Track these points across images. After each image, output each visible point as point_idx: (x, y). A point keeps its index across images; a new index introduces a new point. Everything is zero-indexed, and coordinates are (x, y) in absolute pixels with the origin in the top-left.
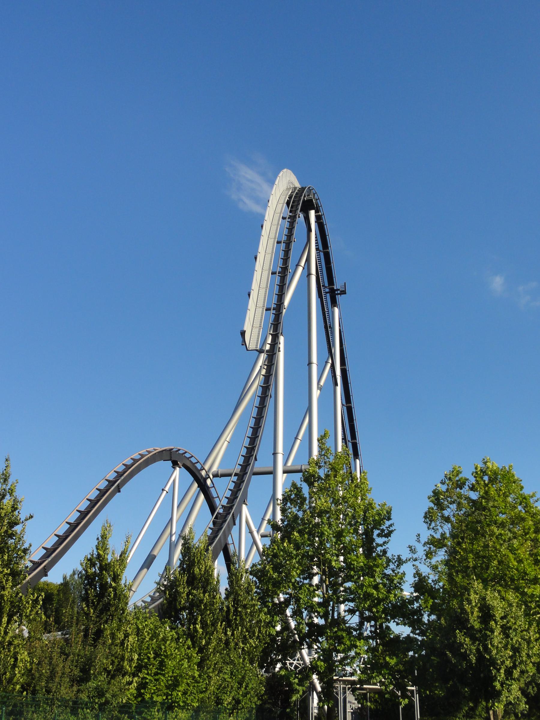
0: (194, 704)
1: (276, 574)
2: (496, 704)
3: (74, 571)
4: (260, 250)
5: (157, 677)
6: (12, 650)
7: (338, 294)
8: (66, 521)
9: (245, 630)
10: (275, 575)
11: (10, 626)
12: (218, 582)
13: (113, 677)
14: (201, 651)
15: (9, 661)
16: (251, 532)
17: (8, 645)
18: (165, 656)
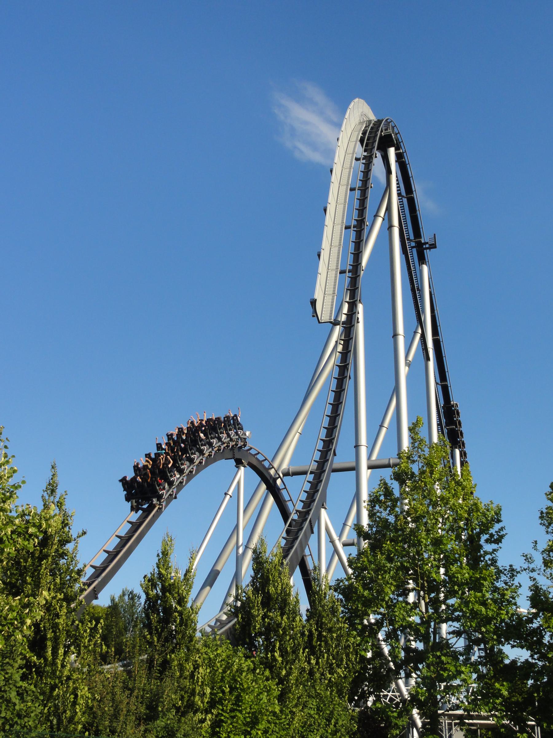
4: (330, 201)
7: (426, 249)
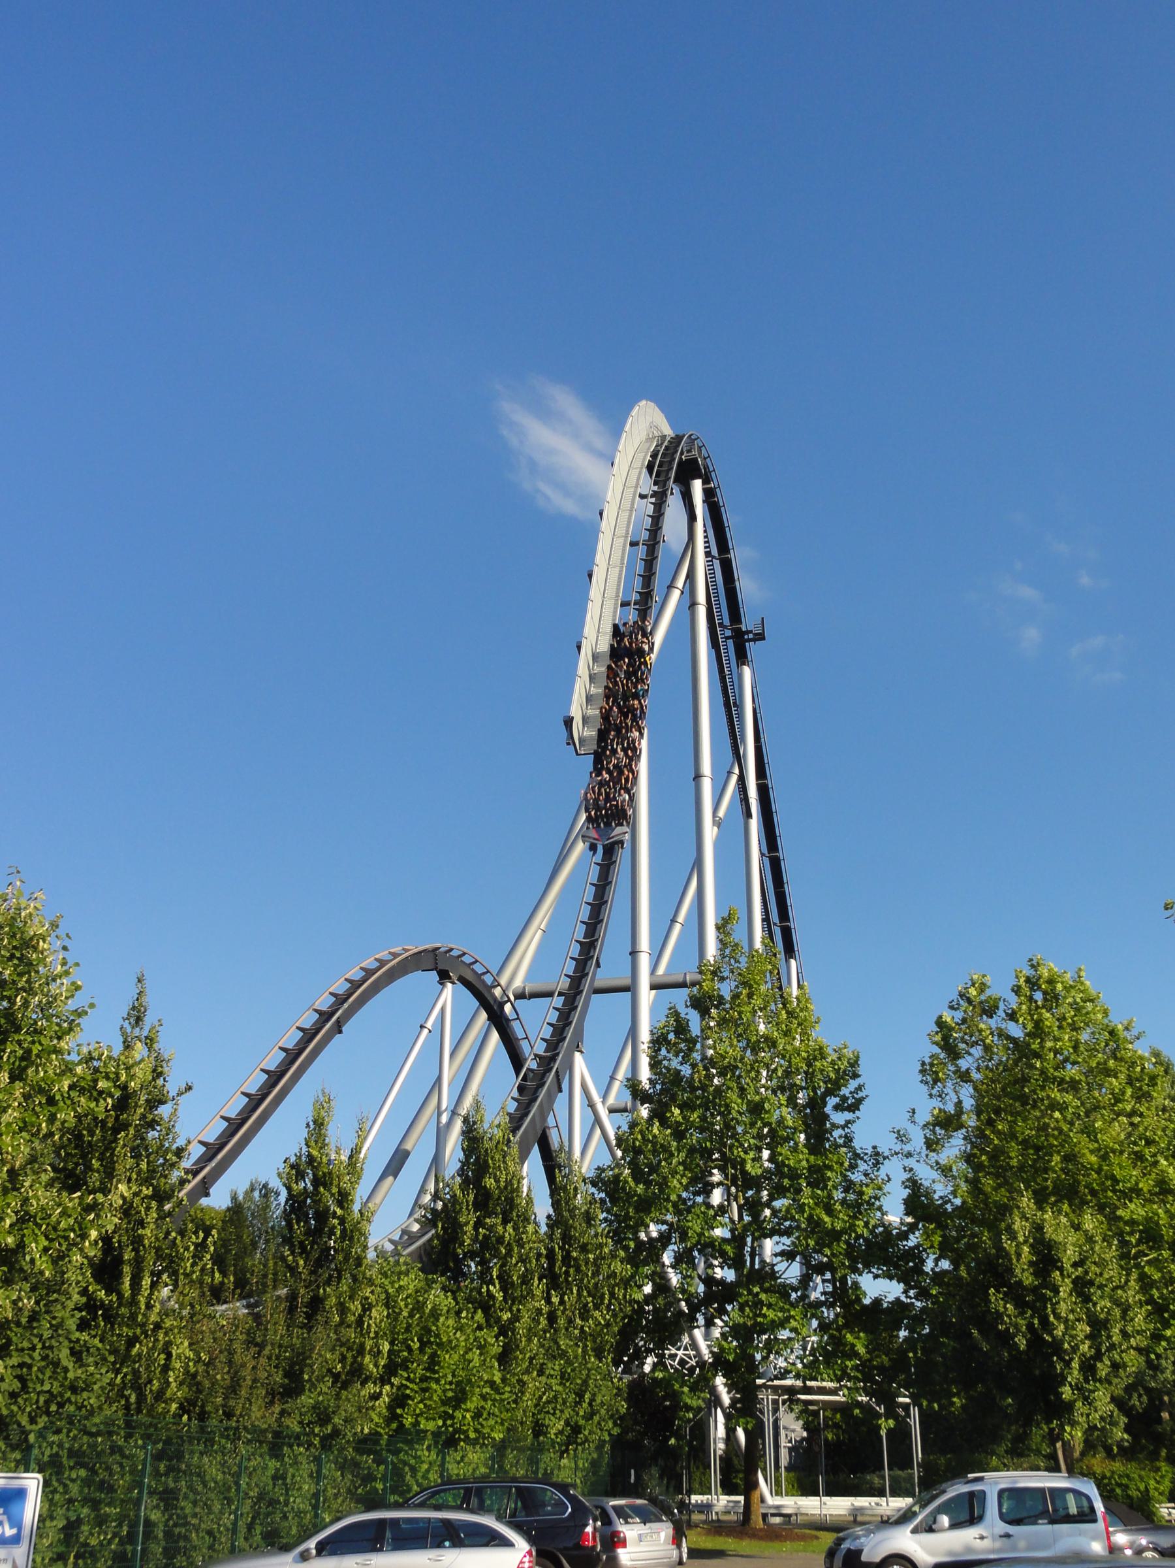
0: (496, 1436)
1: (641, 1186)
2: (1068, 1428)
3: (252, 1183)
4: (597, 561)
5: (424, 1385)
6: (160, 1338)
7: (749, 640)
8: (242, 1089)
9: (585, 1293)
10: (640, 1189)
11: (156, 1293)
12: (530, 1201)
13: (345, 1386)
14: (503, 1331)
15: (155, 1360)
16: (592, 1105)
17: (153, 1330)
18: (437, 1345)
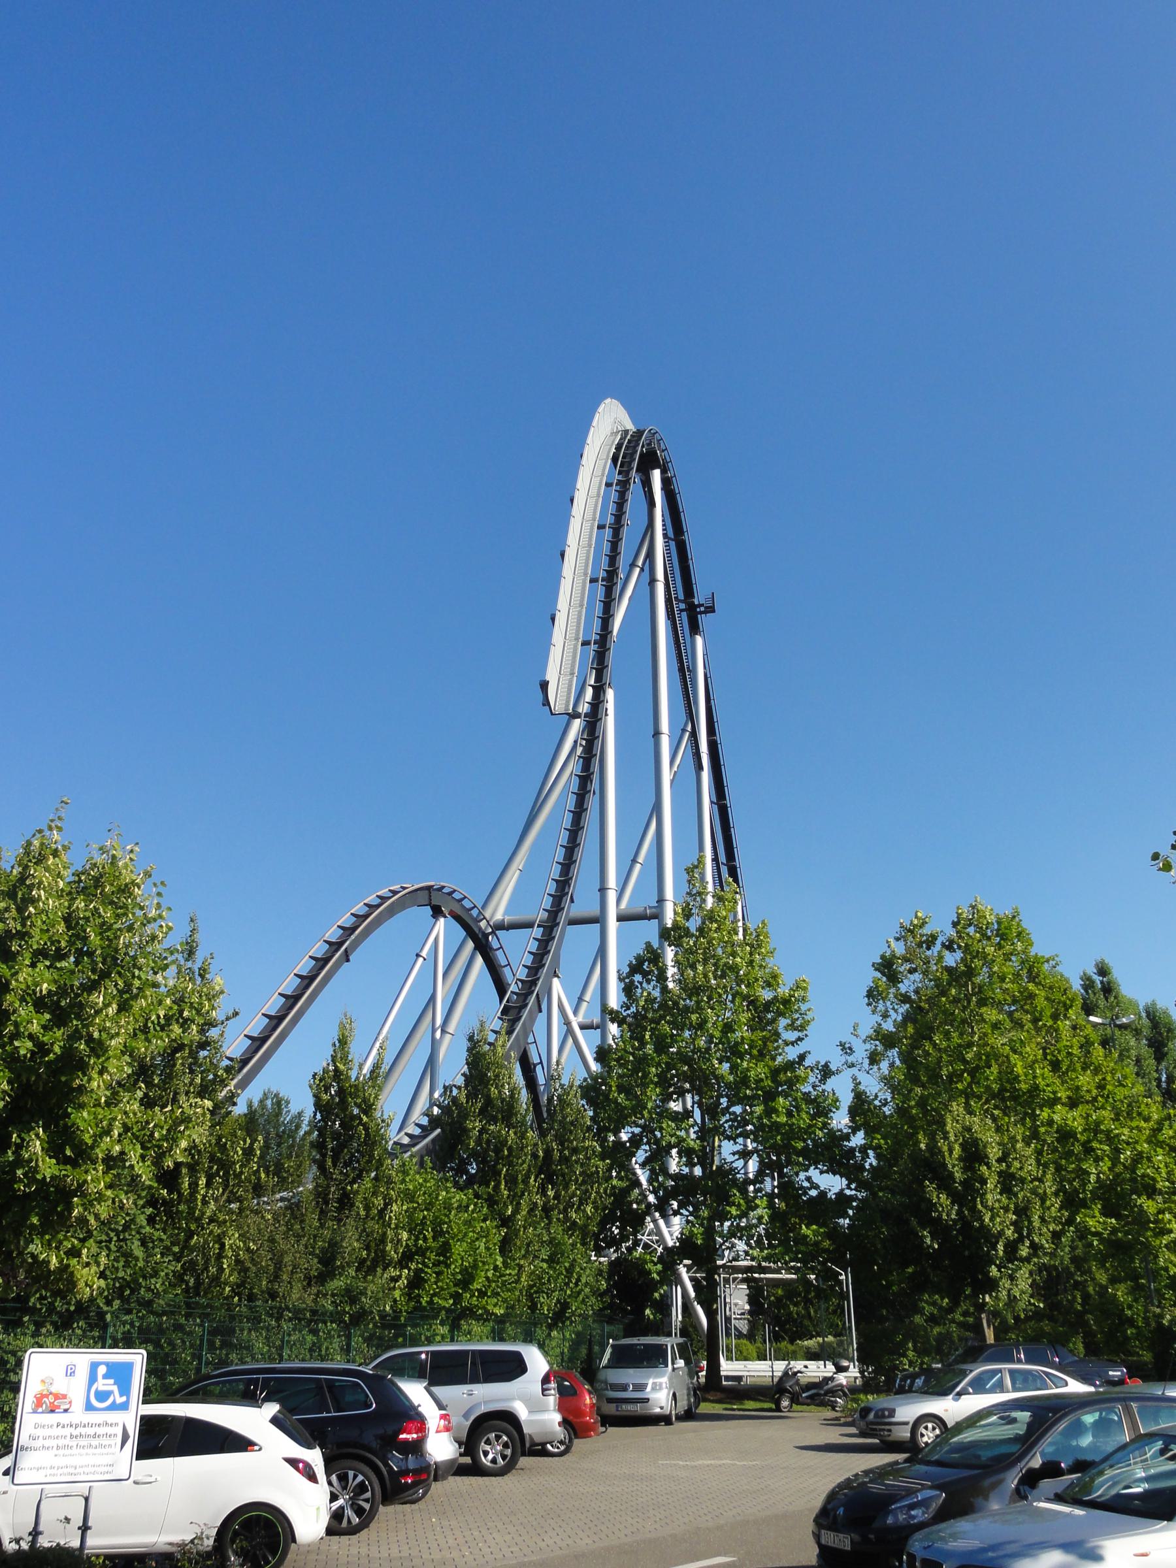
3: (265, 1094)
4: (569, 542)
7: (701, 613)
